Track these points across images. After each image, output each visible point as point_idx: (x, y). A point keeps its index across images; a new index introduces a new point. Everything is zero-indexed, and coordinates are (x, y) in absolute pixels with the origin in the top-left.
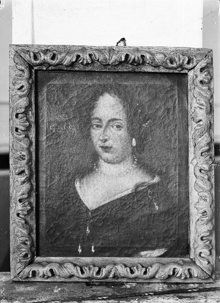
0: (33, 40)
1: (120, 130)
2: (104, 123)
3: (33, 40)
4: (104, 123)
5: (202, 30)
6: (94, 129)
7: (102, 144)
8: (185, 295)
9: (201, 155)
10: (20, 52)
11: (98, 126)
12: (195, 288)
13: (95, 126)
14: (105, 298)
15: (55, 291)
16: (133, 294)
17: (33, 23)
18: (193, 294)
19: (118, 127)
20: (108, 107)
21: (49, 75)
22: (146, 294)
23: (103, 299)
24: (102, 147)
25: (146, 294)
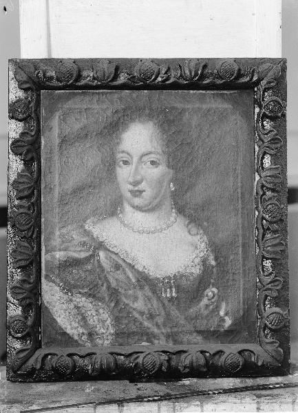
0: (49, 51)
1: (157, 167)
2: (135, 160)
3: (49, 51)
4: (135, 160)
5: (281, 30)
6: (120, 167)
7: (131, 187)
8: (264, 392)
9: (9, 60)
10: (20, 66)
11: (126, 163)
12: (277, 384)
13: (121, 163)
14: (156, 398)
15: (87, 391)
16: (201, 392)
17: (48, 24)
18: (275, 392)
19: (153, 163)
20: (139, 138)
22: (211, 393)
23: (154, 400)
24: (131, 192)
25: (211, 393)
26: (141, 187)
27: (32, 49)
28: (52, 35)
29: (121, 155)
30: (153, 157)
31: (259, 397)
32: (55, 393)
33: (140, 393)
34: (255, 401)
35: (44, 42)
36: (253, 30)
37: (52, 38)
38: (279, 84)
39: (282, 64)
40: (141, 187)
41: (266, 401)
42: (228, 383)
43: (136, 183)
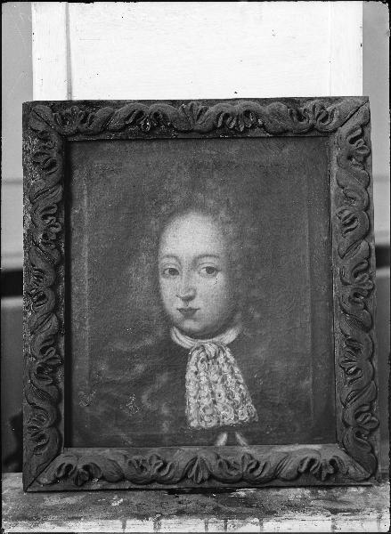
0: (70, 93)
3: (70, 93)
7: (180, 304)
11: (174, 272)
17: (67, 31)
21: (74, 137)
26: (192, 304)
27: (48, 89)
28: (72, 52)
29: (165, 261)
30: (209, 262)
31: (335, 512)
32: (70, 508)
33: (182, 506)
34: (330, 518)
35: (64, 87)
36: (321, 57)
37: (73, 58)
38: (361, 135)
39: (359, 107)
40: (192, 304)
41: (345, 517)
42: (294, 494)
43: (188, 299)
